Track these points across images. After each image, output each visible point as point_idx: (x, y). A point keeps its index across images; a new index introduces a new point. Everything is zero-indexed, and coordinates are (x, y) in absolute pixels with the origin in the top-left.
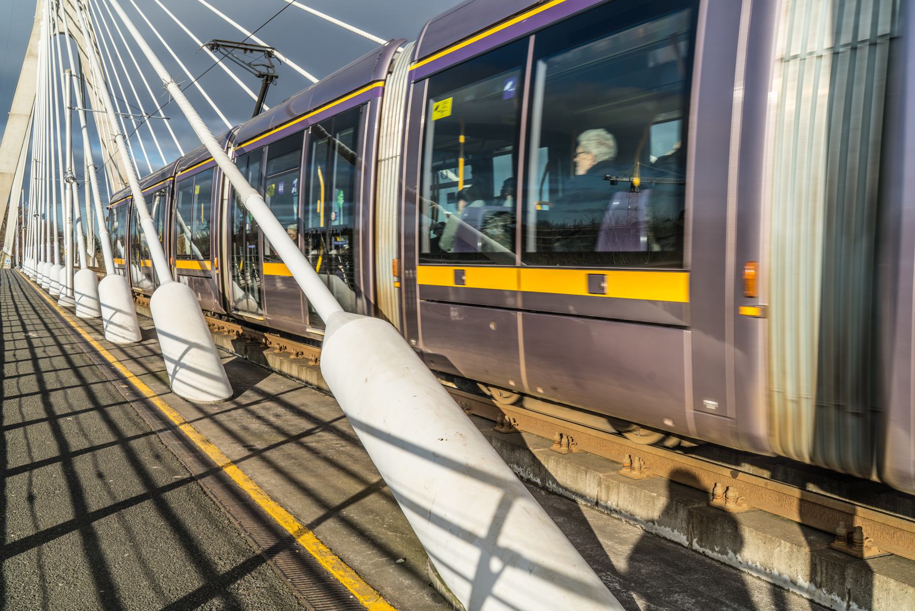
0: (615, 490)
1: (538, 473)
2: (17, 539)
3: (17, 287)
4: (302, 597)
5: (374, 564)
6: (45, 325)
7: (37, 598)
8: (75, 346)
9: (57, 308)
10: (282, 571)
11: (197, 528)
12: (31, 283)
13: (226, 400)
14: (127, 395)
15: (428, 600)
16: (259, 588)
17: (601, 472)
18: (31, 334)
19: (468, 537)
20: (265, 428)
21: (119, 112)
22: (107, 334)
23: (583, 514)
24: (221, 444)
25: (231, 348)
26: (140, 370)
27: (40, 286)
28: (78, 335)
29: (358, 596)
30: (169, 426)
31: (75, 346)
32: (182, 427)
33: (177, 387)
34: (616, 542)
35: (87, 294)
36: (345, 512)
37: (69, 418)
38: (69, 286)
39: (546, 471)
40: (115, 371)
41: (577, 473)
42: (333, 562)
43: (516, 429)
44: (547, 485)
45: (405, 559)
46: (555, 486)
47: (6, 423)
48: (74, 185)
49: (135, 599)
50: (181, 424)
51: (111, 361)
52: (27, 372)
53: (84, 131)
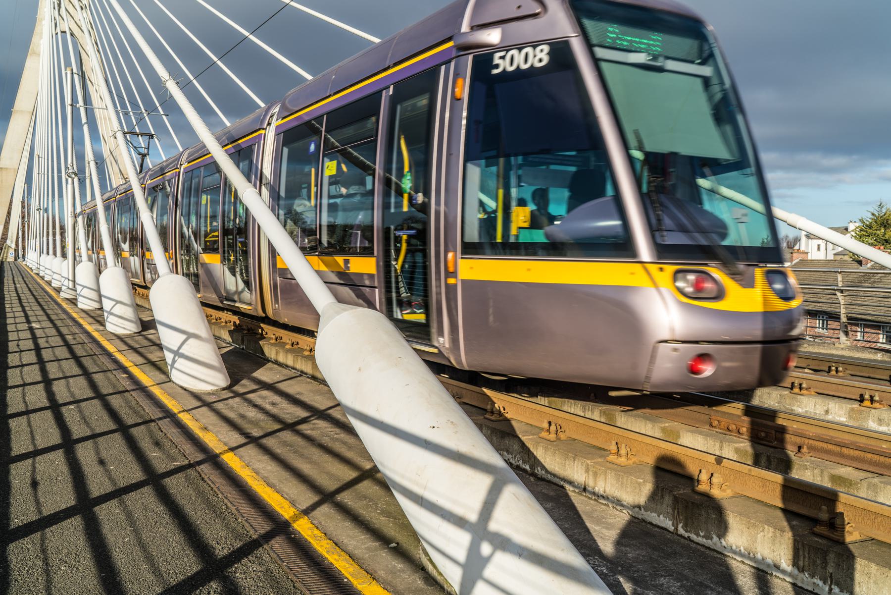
0: (603, 476)
2: (20, 524)
3: (20, 279)
4: (298, 580)
5: (368, 549)
6: (48, 316)
7: (40, 581)
9: (59, 300)
11: (196, 513)
12: (34, 275)
13: (224, 389)
14: (127, 384)
15: (420, 583)
17: (588, 459)
18: (34, 325)
19: (459, 522)
20: (261, 416)
21: (119, 109)
23: (571, 500)
25: (228, 338)
26: (140, 360)
27: (42, 278)
28: (80, 326)
30: (168, 414)
33: (176, 376)
34: (603, 528)
35: (88, 286)
36: (339, 498)
37: (71, 407)
38: (71, 278)
39: (535, 457)
40: (116, 361)
41: (565, 460)
42: (328, 546)
43: (506, 418)
44: (536, 471)
45: (398, 544)
46: (543, 472)
47: (10, 411)
49: (135, 582)
50: (180, 412)
51: (112, 351)
52: (30, 362)
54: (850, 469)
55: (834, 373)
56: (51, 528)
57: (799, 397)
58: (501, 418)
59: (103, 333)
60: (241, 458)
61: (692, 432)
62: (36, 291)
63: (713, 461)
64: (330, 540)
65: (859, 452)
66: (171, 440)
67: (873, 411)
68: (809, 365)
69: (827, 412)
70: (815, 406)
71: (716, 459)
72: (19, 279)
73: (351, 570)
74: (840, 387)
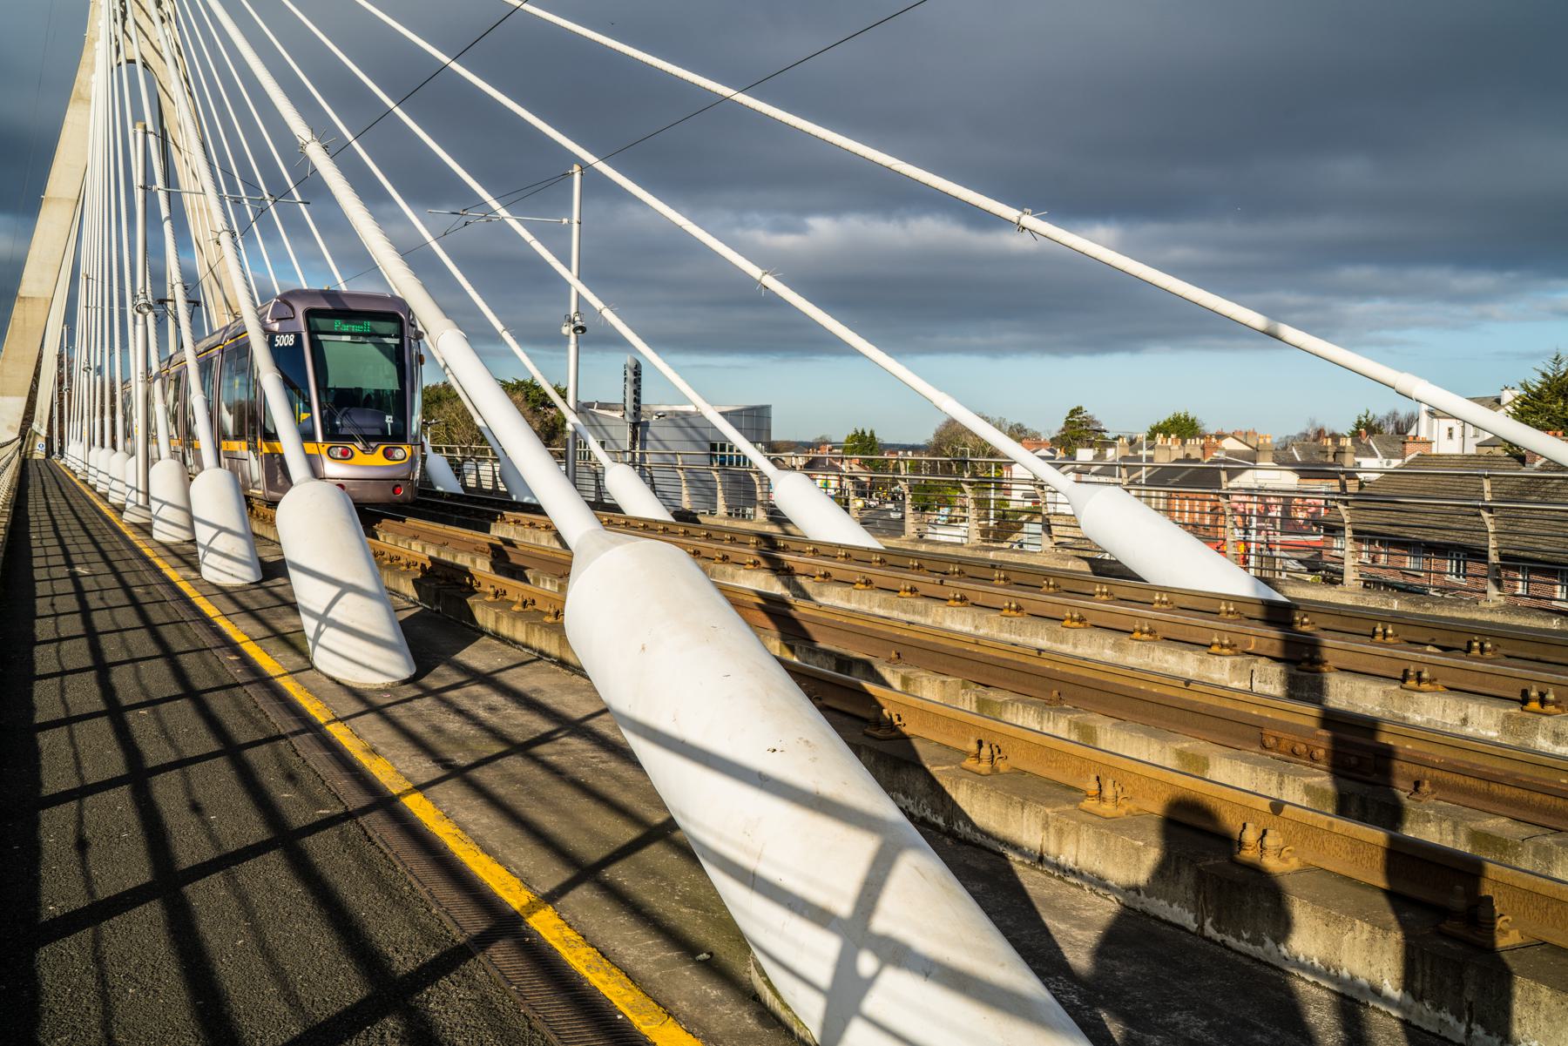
0: (1072, 837)
1: (939, 807)
2: (58, 914)
8: (151, 589)
9: (121, 526)
10: (502, 973)
11: (358, 898)
12: (79, 484)
13: (405, 682)
15: (750, 1023)
16: (463, 1000)
18: (78, 569)
19: (820, 916)
20: (470, 730)
21: (225, 193)
22: (204, 568)
24: (396, 757)
25: (411, 592)
27: (93, 488)
28: (158, 571)
29: (630, 1016)
30: (309, 725)
31: (151, 589)
32: (330, 728)
33: (321, 659)
34: (1074, 926)
35: (171, 502)
38: (141, 488)
39: (954, 804)
40: (218, 633)
41: (1007, 807)
42: (588, 958)
44: (956, 828)
45: (711, 954)
46: (968, 830)
47: (39, 718)
48: (150, 317)
49: (255, 1016)
50: (329, 722)
52: (72, 634)
53: (167, 226)
54: (1504, 820)
55: (1476, 652)
56: (111, 921)
57: (1416, 695)
58: (894, 734)
59: (195, 582)
60: (435, 803)
61: (1230, 757)
62: (83, 511)
63: (1267, 808)
64: (593, 946)
65: (1521, 791)
66: (314, 771)
67: (1545, 719)
68: (1434, 640)
69: (1465, 721)
70: (1444, 711)
71: (1271, 805)
72: (52, 490)
73: (629, 999)
74: (1488, 677)
